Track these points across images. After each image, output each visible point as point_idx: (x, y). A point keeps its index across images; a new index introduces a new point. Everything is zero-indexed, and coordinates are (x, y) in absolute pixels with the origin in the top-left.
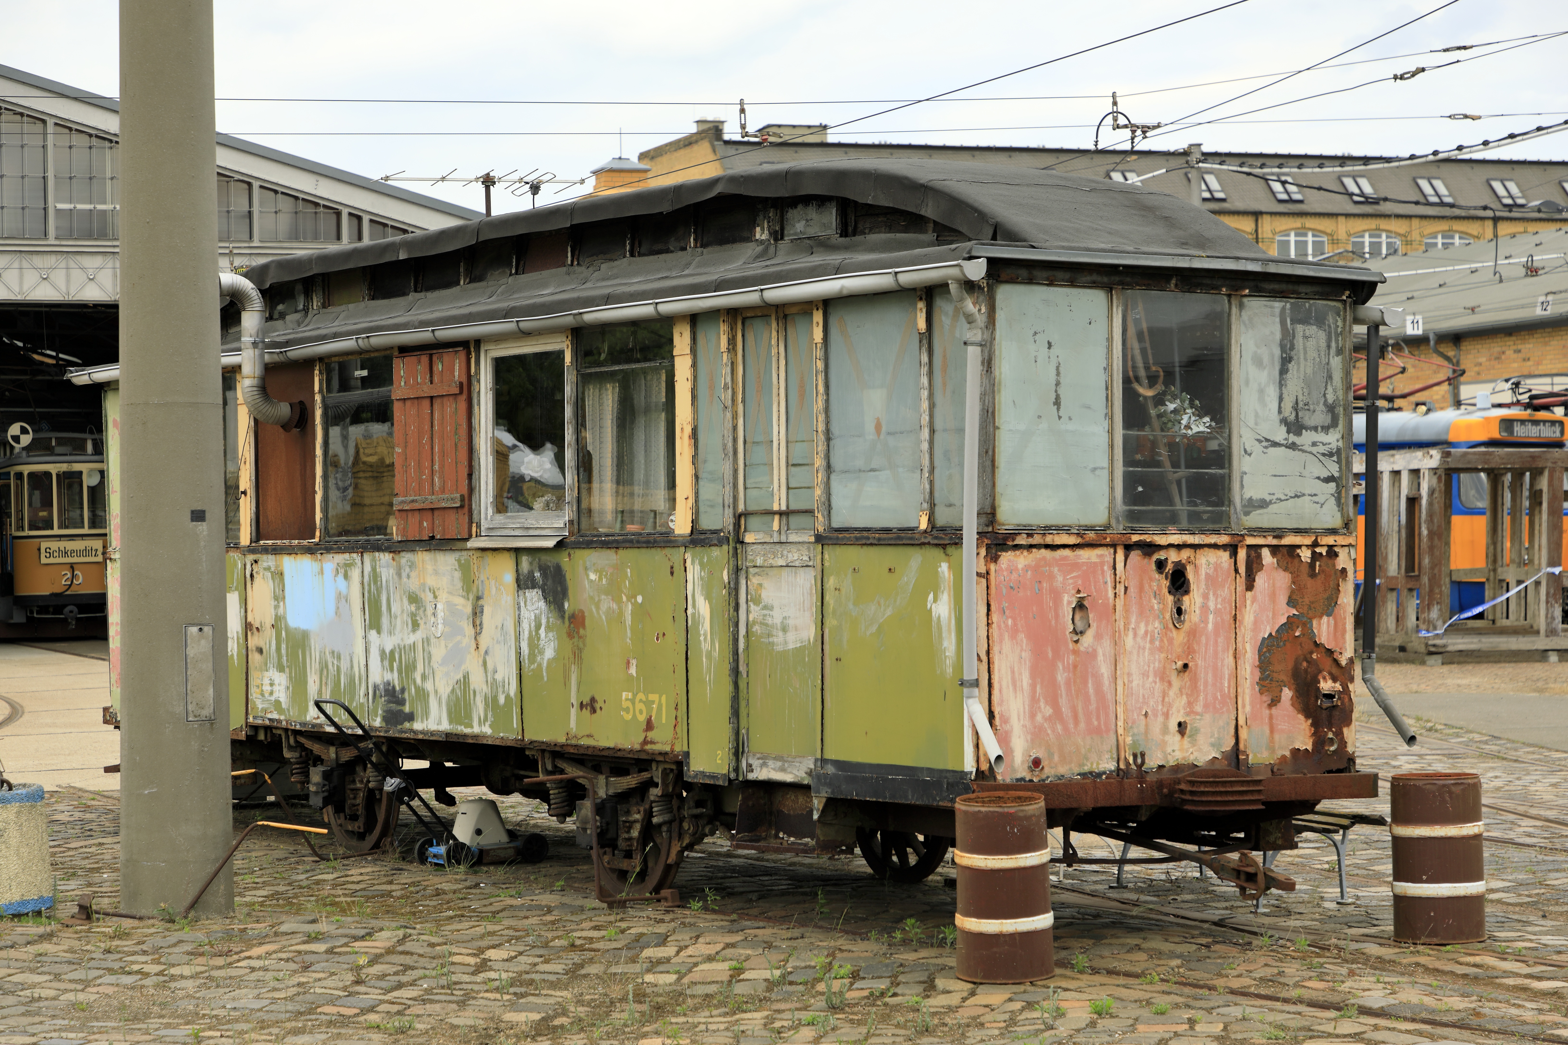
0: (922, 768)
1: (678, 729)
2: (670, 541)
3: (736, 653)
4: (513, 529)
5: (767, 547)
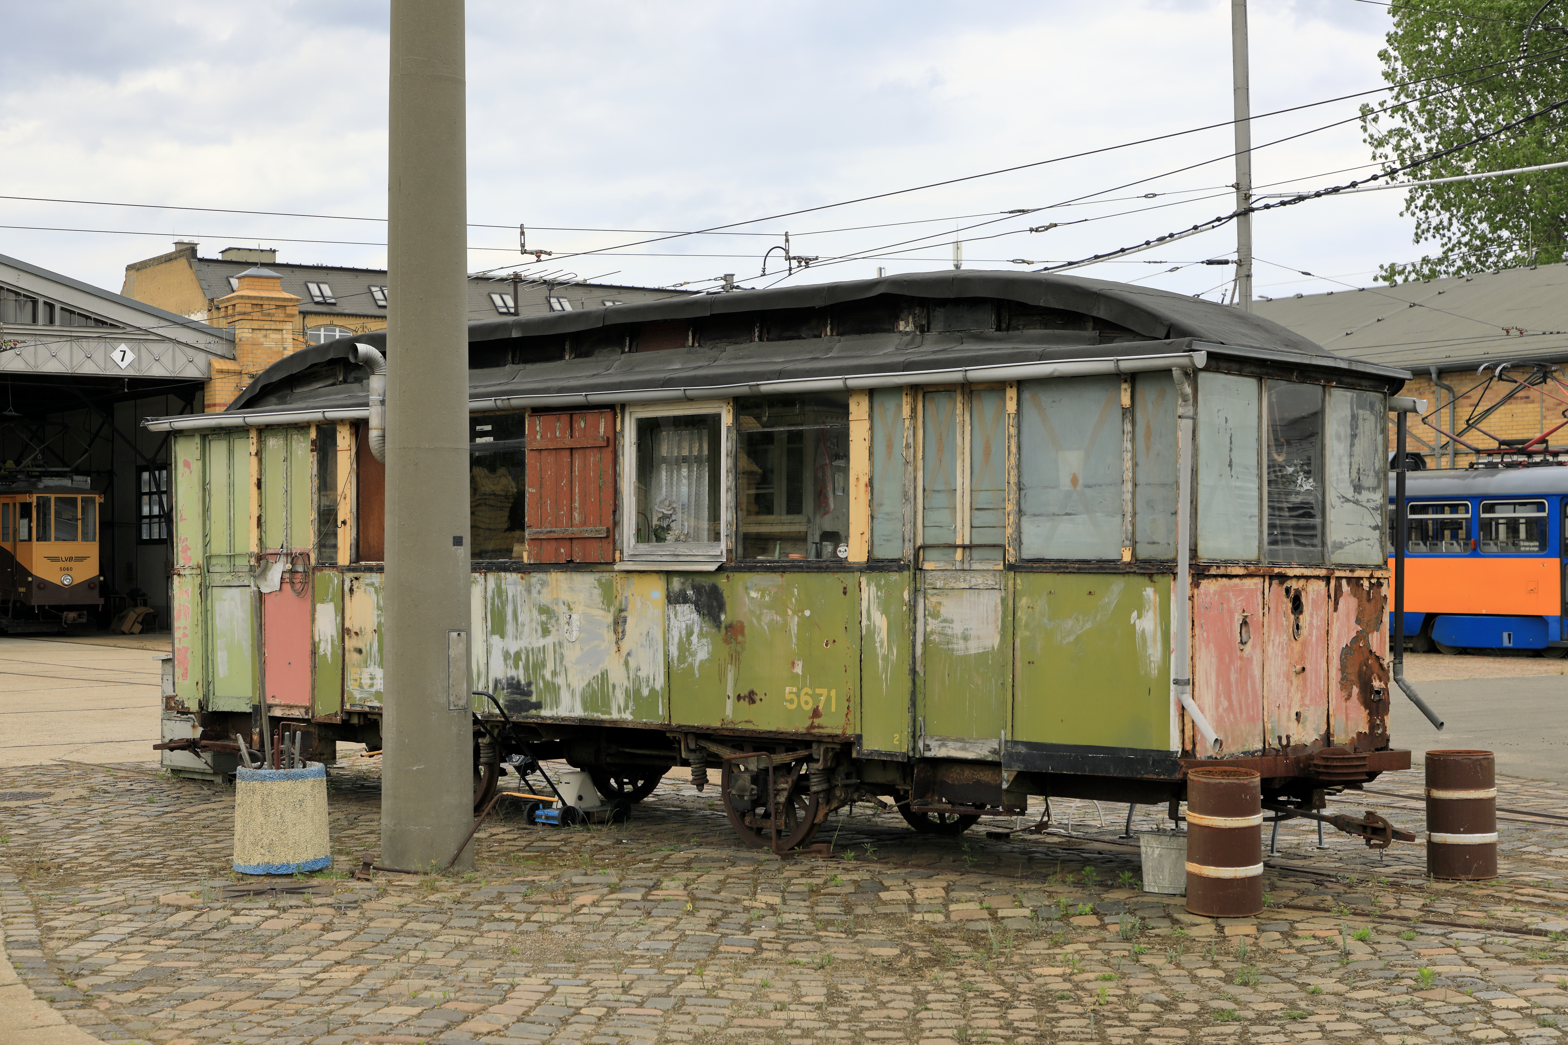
0: (1124, 749)
1: (850, 717)
2: (845, 568)
3: (914, 657)
4: (661, 556)
5: (948, 573)
